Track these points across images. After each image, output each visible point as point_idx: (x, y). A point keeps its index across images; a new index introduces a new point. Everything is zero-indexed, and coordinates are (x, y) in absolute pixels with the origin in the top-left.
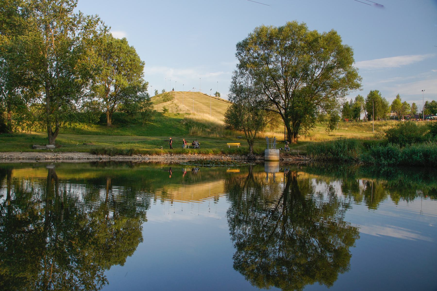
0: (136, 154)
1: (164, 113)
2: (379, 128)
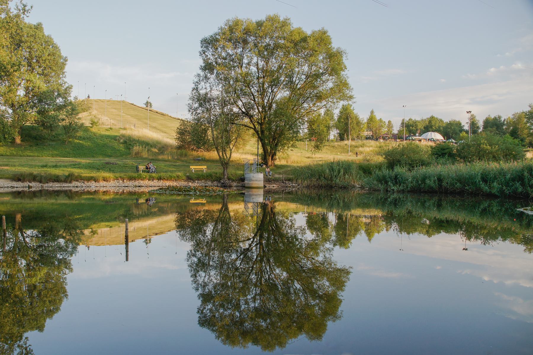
0: (77, 181)
1: (91, 127)
2: (356, 149)
